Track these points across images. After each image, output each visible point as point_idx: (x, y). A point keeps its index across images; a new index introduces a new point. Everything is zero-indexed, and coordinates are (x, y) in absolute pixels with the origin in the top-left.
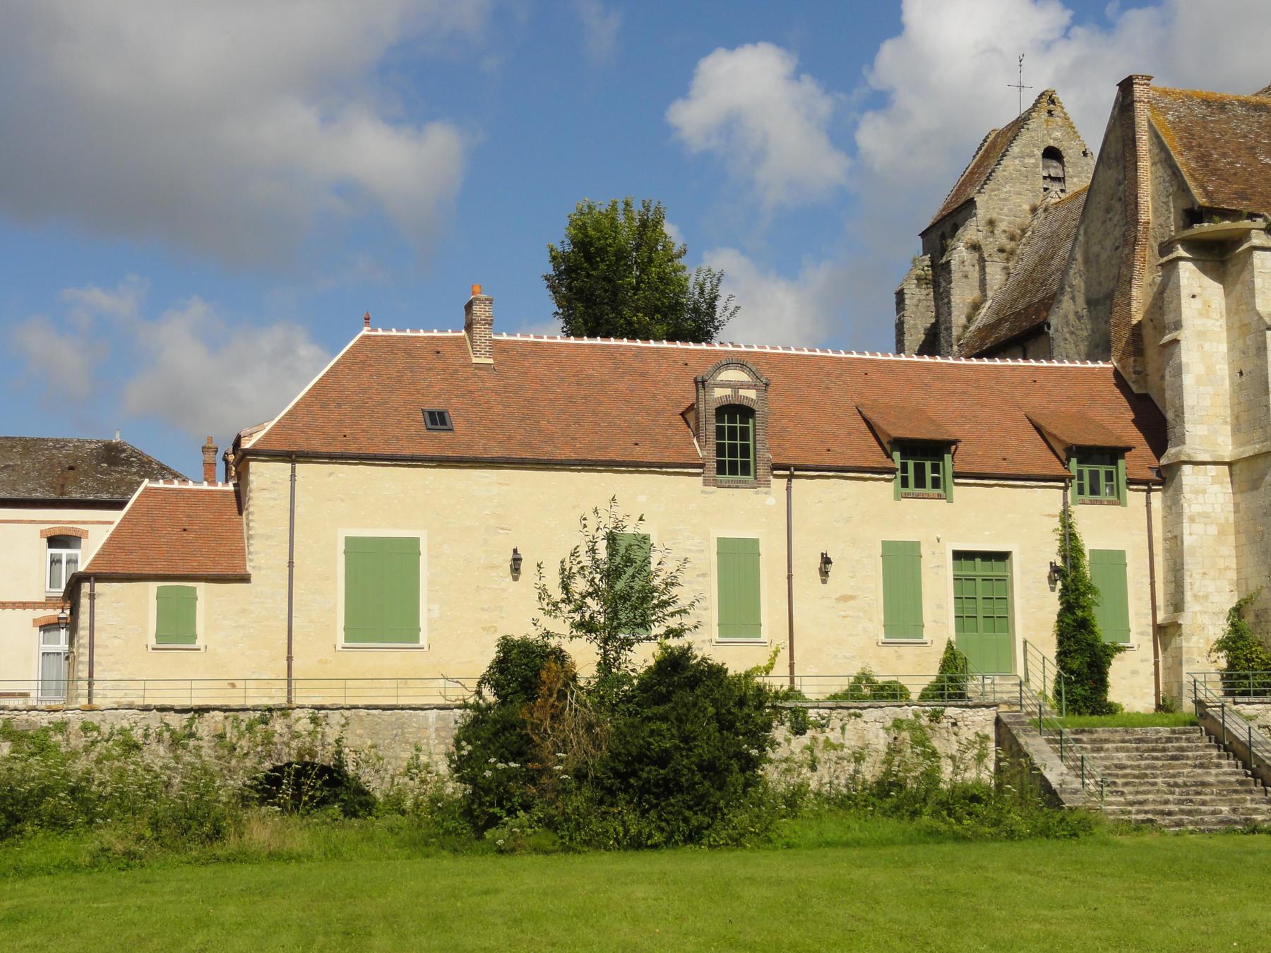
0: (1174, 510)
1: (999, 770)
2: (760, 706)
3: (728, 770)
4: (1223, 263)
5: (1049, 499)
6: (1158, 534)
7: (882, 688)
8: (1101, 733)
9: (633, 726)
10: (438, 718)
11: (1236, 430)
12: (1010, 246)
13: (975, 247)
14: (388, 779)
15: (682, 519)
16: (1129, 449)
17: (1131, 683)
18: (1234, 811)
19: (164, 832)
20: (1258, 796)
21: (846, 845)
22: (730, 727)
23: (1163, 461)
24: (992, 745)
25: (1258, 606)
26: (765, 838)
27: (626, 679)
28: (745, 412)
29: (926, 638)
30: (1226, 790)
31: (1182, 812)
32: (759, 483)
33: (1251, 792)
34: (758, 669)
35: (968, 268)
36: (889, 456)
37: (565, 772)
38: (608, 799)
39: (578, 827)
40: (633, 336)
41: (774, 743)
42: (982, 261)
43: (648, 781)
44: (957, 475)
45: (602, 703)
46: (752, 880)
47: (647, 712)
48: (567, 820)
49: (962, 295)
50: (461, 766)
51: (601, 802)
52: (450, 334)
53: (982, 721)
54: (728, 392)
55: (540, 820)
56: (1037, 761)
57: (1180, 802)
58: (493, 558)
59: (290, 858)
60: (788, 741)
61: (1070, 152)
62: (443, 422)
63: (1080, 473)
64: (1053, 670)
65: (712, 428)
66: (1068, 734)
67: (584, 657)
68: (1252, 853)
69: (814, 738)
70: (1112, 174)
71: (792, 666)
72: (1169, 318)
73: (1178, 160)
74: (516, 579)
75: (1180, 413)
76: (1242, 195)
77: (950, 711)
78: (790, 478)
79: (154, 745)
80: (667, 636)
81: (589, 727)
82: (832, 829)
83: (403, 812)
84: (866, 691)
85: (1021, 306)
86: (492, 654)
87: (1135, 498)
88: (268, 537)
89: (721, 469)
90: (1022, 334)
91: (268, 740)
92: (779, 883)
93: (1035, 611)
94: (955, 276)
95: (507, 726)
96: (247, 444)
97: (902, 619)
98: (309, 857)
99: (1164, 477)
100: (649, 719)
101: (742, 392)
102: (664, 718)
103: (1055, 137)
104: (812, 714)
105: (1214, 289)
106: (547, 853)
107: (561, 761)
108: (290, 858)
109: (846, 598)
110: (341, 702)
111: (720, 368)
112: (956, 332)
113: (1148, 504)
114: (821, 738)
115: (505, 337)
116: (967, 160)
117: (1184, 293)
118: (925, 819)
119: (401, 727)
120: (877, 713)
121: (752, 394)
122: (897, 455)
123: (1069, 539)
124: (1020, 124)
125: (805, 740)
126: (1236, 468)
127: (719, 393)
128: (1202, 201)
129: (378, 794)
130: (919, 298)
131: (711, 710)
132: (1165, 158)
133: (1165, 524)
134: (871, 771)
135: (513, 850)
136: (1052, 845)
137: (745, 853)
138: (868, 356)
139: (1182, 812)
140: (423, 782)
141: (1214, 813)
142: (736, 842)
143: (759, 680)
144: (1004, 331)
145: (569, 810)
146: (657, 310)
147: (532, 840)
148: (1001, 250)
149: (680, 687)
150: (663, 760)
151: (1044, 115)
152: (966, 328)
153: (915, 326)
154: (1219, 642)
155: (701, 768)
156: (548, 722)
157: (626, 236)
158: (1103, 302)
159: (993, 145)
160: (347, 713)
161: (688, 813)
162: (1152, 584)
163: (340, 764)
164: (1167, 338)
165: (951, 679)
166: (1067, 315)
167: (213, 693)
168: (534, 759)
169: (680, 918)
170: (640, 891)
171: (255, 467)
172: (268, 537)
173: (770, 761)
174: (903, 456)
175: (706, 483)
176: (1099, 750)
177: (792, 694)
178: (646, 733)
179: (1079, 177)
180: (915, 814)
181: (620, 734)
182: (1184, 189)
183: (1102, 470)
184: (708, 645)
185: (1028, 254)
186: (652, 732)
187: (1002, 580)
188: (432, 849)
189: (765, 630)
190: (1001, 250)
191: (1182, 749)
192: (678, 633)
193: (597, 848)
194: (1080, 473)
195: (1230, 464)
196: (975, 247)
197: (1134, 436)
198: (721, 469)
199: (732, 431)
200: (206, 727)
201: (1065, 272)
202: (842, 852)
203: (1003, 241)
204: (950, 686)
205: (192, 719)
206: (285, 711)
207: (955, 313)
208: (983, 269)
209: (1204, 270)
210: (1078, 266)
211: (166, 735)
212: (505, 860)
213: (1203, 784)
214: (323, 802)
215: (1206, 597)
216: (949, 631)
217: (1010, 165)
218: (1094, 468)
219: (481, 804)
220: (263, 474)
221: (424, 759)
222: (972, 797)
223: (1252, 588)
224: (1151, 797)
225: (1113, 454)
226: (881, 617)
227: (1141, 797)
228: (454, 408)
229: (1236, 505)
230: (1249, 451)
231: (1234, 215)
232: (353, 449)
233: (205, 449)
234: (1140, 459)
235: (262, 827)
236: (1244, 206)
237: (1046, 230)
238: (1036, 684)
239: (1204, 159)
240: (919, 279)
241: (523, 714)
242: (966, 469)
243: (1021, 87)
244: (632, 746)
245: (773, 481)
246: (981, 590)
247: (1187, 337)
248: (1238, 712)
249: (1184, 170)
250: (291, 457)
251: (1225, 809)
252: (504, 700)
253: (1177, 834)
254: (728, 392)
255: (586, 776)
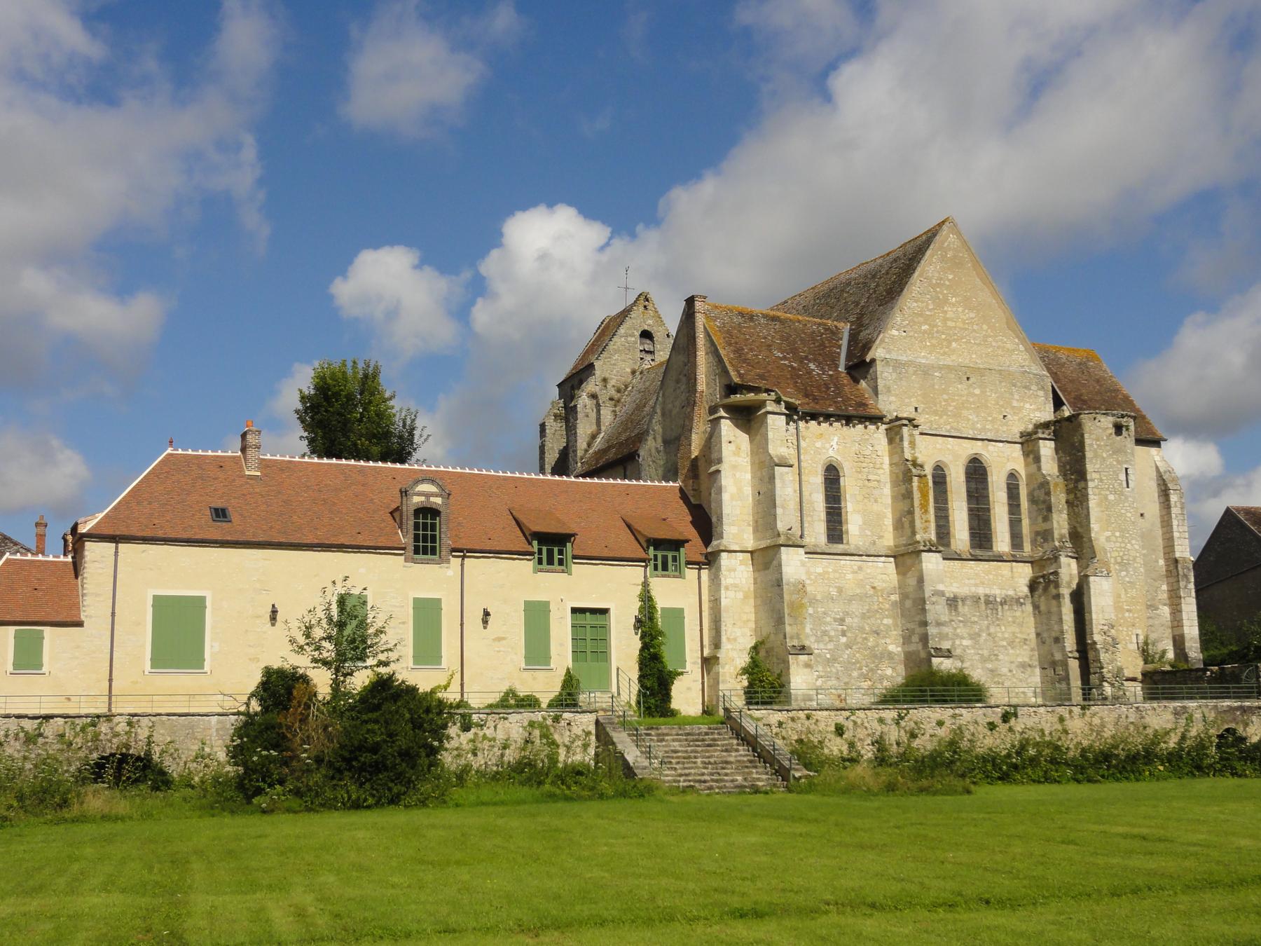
0: (715, 581)
1: (597, 755)
2: (440, 713)
3: (418, 755)
4: (749, 421)
5: (633, 575)
6: (705, 597)
7: (523, 700)
8: (664, 729)
9: (355, 726)
10: (219, 722)
11: (756, 530)
12: (617, 396)
13: (594, 396)
14: (182, 764)
15: (390, 585)
16: (687, 541)
17: (686, 696)
18: (745, 779)
19: (28, 802)
20: (761, 770)
21: (495, 804)
22: (420, 727)
23: (709, 550)
24: (593, 738)
25: (768, 645)
26: (442, 801)
27: (348, 694)
28: (433, 512)
29: (552, 666)
30: (741, 766)
31: (713, 780)
32: (442, 561)
33: (756, 767)
34: (439, 687)
35: (589, 410)
36: (530, 544)
37: (308, 758)
38: (337, 776)
39: (317, 795)
40: (358, 457)
41: (449, 738)
42: (598, 406)
43: (364, 763)
44: (574, 557)
45: (334, 711)
46: (433, 826)
47: (365, 717)
48: (310, 790)
49: (584, 429)
50: (237, 753)
51: (333, 778)
52: (230, 454)
53: (585, 722)
54: (423, 499)
55: (290, 791)
56: (620, 747)
57: (712, 774)
58: (257, 613)
59: (117, 819)
60: (459, 736)
61: (658, 335)
62: (225, 516)
63: (656, 556)
64: (635, 687)
65: (411, 523)
66: (642, 730)
67: (322, 680)
68: (749, 806)
69: (476, 734)
70: (681, 358)
71: (462, 685)
72: (714, 456)
73: (722, 352)
74: (273, 625)
75: (720, 518)
76: (762, 377)
77: (566, 715)
78: (463, 557)
79: (12, 742)
80: (378, 666)
81: (325, 728)
82: (486, 794)
83: (193, 787)
84: (512, 702)
85: (623, 438)
86: (257, 678)
87: (691, 573)
88: (97, 595)
89: (416, 552)
90: (619, 460)
91: (96, 737)
92: (450, 827)
93: (624, 648)
94: (580, 415)
95: (270, 727)
96: (83, 529)
97: (537, 653)
98: (131, 818)
99: (710, 560)
100: (366, 722)
101: (432, 499)
102: (376, 721)
103: (649, 325)
104: (475, 718)
105: (743, 438)
106: (295, 812)
107: (306, 751)
108: (117, 819)
109: (499, 639)
110: (149, 711)
111: (417, 482)
112: (580, 453)
113: (699, 578)
114: (481, 734)
115: (268, 457)
116: (590, 335)
117: (724, 439)
118: (547, 787)
119: (192, 728)
120: (518, 717)
121: (439, 500)
122: (535, 543)
123: (647, 599)
124: (625, 313)
125: (470, 735)
126: (756, 555)
127: (416, 499)
128: (736, 380)
129: (175, 775)
130: (555, 429)
131: (407, 716)
132: (714, 351)
133: (710, 591)
134: (511, 756)
135: (272, 811)
136: (627, 802)
137: (428, 810)
138: (517, 475)
139: (713, 780)
140: (206, 766)
141: (732, 781)
142: (423, 803)
143: (440, 695)
144: (611, 455)
145: (311, 783)
146: (374, 436)
147: (286, 804)
148: (611, 399)
149: (386, 699)
150: (375, 749)
151: (641, 309)
152: (586, 451)
153: (552, 448)
154: (744, 669)
155: (400, 754)
156: (297, 725)
157: (354, 387)
158: (675, 441)
159: (607, 326)
160: (153, 719)
161: (391, 785)
162: (701, 630)
163: (148, 754)
164: (713, 469)
165: (569, 694)
166: (650, 449)
167: (53, 705)
168: (288, 749)
169: (388, 848)
170: (360, 834)
171: (89, 546)
172: (97, 595)
173: (446, 750)
174: (539, 544)
175: (406, 561)
176: (662, 740)
177: (462, 704)
178: (364, 731)
179: (663, 354)
180: (540, 783)
181: (346, 732)
182: (726, 372)
183: (670, 555)
184: (408, 673)
185: (628, 400)
186: (368, 731)
187: (603, 627)
188: (216, 811)
189: (444, 660)
190: (611, 399)
191: (714, 740)
192: (385, 664)
193: (330, 808)
194: (656, 556)
195: (751, 552)
196: (594, 396)
197: (691, 533)
198: (416, 552)
199: (425, 525)
200: (50, 730)
201: (650, 421)
202: (491, 809)
203: (613, 392)
204: (568, 699)
205: (41, 723)
206: (109, 717)
207: (579, 441)
208: (598, 411)
209: (737, 426)
210: (658, 417)
211: (22, 735)
212: (266, 818)
213: (727, 762)
214: (137, 781)
215: (735, 640)
216: (569, 662)
217: (618, 341)
218: (665, 553)
219: (251, 780)
220: (93, 550)
221: (207, 750)
222: (577, 772)
223: (764, 634)
224: (692, 771)
225: (676, 545)
226: (522, 651)
227: (687, 771)
228: (232, 506)
229: (755, 579)
230: (763, 544)
231: (756, 390)
232: (160, 534)
233: (37, 525)
234: (694, 548)
235: (97, 799)
236: (762, 384)
237: (640, 386)
238: (624, 697)
239: (738, 351)
240: (555, 416)
241: (280, 719)
242: (581, 553)
243: (626, 288)
244: (352, 744)
245: (452, 559)
246: (589, 634)
247: (725, 468)
248: (751, 717)
249: (725, 359)
250: (115, 539)
251: (739, 778)
252: (266, 709)
253: (708, 795)
254: (423, 499)
255: (323, 761)
